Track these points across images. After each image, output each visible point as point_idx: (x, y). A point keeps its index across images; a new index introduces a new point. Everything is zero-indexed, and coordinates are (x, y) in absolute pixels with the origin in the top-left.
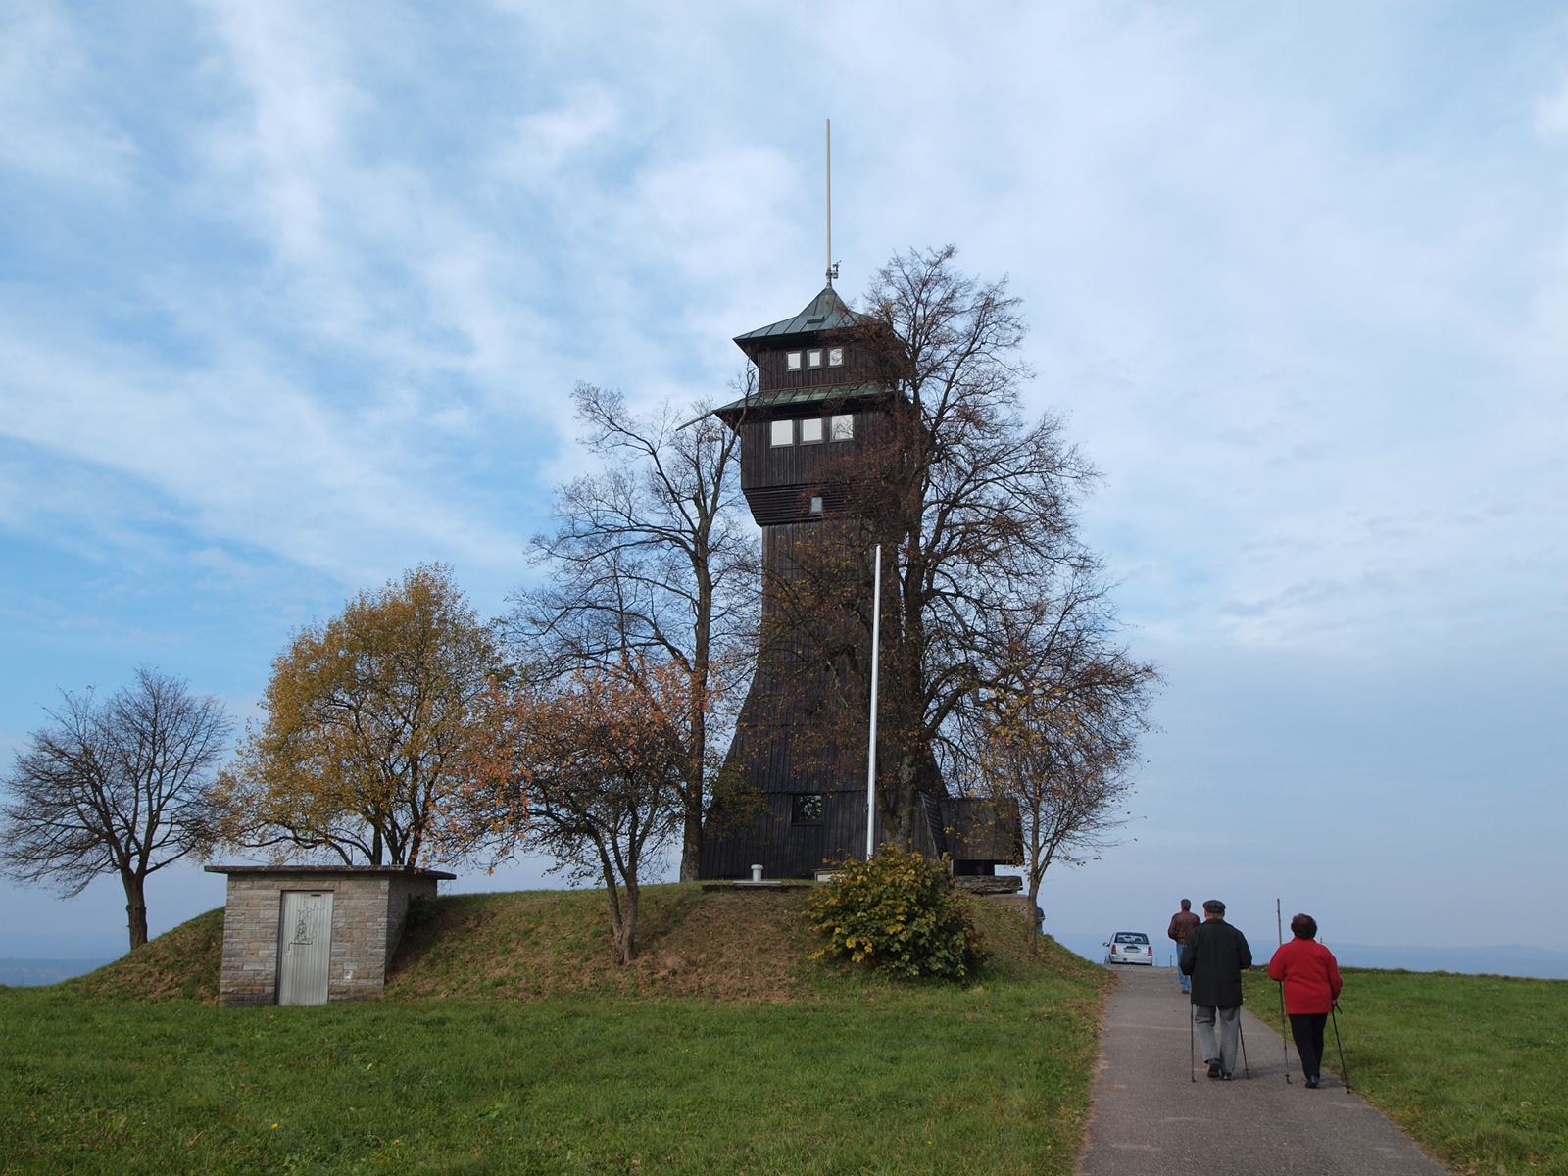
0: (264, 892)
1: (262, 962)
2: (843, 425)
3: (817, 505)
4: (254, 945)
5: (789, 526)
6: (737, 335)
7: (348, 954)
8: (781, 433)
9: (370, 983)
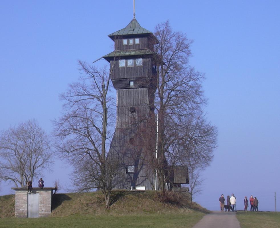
0: (24, 193)
1: (24, 208)
2: (140, 62)
3: (132, 84)
4: (22, 205)
5: (124, 90)
6: (110, 33)
7: (43, 206)
8: (122, 63)
9: (48, 213)
